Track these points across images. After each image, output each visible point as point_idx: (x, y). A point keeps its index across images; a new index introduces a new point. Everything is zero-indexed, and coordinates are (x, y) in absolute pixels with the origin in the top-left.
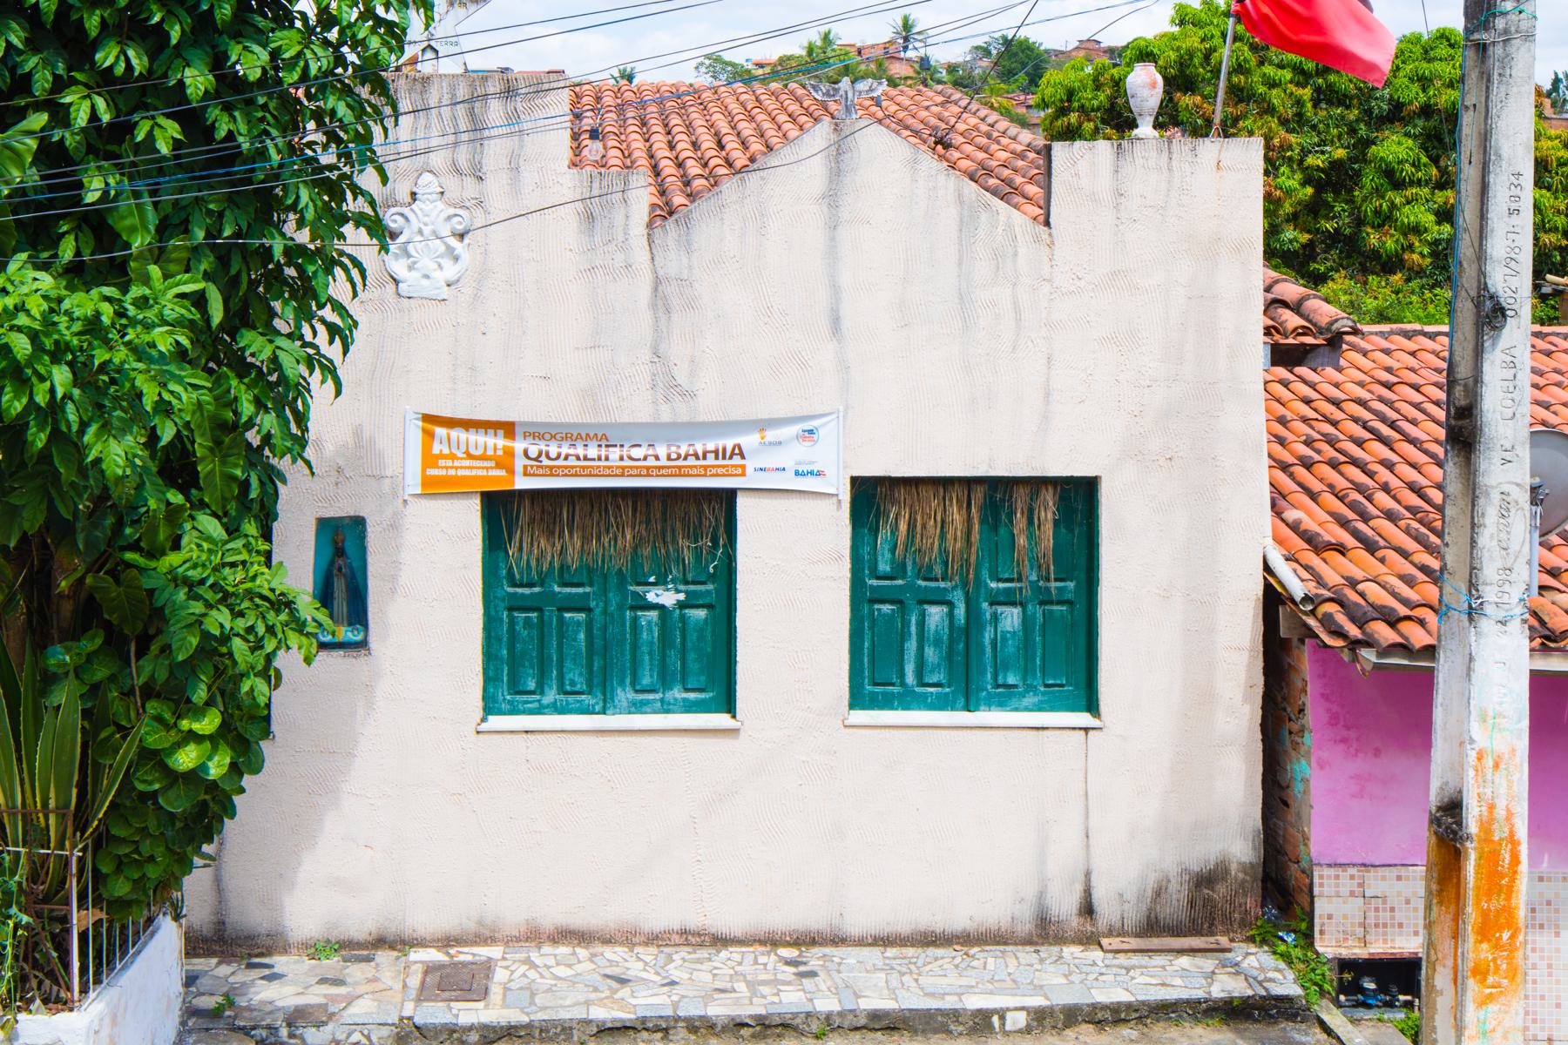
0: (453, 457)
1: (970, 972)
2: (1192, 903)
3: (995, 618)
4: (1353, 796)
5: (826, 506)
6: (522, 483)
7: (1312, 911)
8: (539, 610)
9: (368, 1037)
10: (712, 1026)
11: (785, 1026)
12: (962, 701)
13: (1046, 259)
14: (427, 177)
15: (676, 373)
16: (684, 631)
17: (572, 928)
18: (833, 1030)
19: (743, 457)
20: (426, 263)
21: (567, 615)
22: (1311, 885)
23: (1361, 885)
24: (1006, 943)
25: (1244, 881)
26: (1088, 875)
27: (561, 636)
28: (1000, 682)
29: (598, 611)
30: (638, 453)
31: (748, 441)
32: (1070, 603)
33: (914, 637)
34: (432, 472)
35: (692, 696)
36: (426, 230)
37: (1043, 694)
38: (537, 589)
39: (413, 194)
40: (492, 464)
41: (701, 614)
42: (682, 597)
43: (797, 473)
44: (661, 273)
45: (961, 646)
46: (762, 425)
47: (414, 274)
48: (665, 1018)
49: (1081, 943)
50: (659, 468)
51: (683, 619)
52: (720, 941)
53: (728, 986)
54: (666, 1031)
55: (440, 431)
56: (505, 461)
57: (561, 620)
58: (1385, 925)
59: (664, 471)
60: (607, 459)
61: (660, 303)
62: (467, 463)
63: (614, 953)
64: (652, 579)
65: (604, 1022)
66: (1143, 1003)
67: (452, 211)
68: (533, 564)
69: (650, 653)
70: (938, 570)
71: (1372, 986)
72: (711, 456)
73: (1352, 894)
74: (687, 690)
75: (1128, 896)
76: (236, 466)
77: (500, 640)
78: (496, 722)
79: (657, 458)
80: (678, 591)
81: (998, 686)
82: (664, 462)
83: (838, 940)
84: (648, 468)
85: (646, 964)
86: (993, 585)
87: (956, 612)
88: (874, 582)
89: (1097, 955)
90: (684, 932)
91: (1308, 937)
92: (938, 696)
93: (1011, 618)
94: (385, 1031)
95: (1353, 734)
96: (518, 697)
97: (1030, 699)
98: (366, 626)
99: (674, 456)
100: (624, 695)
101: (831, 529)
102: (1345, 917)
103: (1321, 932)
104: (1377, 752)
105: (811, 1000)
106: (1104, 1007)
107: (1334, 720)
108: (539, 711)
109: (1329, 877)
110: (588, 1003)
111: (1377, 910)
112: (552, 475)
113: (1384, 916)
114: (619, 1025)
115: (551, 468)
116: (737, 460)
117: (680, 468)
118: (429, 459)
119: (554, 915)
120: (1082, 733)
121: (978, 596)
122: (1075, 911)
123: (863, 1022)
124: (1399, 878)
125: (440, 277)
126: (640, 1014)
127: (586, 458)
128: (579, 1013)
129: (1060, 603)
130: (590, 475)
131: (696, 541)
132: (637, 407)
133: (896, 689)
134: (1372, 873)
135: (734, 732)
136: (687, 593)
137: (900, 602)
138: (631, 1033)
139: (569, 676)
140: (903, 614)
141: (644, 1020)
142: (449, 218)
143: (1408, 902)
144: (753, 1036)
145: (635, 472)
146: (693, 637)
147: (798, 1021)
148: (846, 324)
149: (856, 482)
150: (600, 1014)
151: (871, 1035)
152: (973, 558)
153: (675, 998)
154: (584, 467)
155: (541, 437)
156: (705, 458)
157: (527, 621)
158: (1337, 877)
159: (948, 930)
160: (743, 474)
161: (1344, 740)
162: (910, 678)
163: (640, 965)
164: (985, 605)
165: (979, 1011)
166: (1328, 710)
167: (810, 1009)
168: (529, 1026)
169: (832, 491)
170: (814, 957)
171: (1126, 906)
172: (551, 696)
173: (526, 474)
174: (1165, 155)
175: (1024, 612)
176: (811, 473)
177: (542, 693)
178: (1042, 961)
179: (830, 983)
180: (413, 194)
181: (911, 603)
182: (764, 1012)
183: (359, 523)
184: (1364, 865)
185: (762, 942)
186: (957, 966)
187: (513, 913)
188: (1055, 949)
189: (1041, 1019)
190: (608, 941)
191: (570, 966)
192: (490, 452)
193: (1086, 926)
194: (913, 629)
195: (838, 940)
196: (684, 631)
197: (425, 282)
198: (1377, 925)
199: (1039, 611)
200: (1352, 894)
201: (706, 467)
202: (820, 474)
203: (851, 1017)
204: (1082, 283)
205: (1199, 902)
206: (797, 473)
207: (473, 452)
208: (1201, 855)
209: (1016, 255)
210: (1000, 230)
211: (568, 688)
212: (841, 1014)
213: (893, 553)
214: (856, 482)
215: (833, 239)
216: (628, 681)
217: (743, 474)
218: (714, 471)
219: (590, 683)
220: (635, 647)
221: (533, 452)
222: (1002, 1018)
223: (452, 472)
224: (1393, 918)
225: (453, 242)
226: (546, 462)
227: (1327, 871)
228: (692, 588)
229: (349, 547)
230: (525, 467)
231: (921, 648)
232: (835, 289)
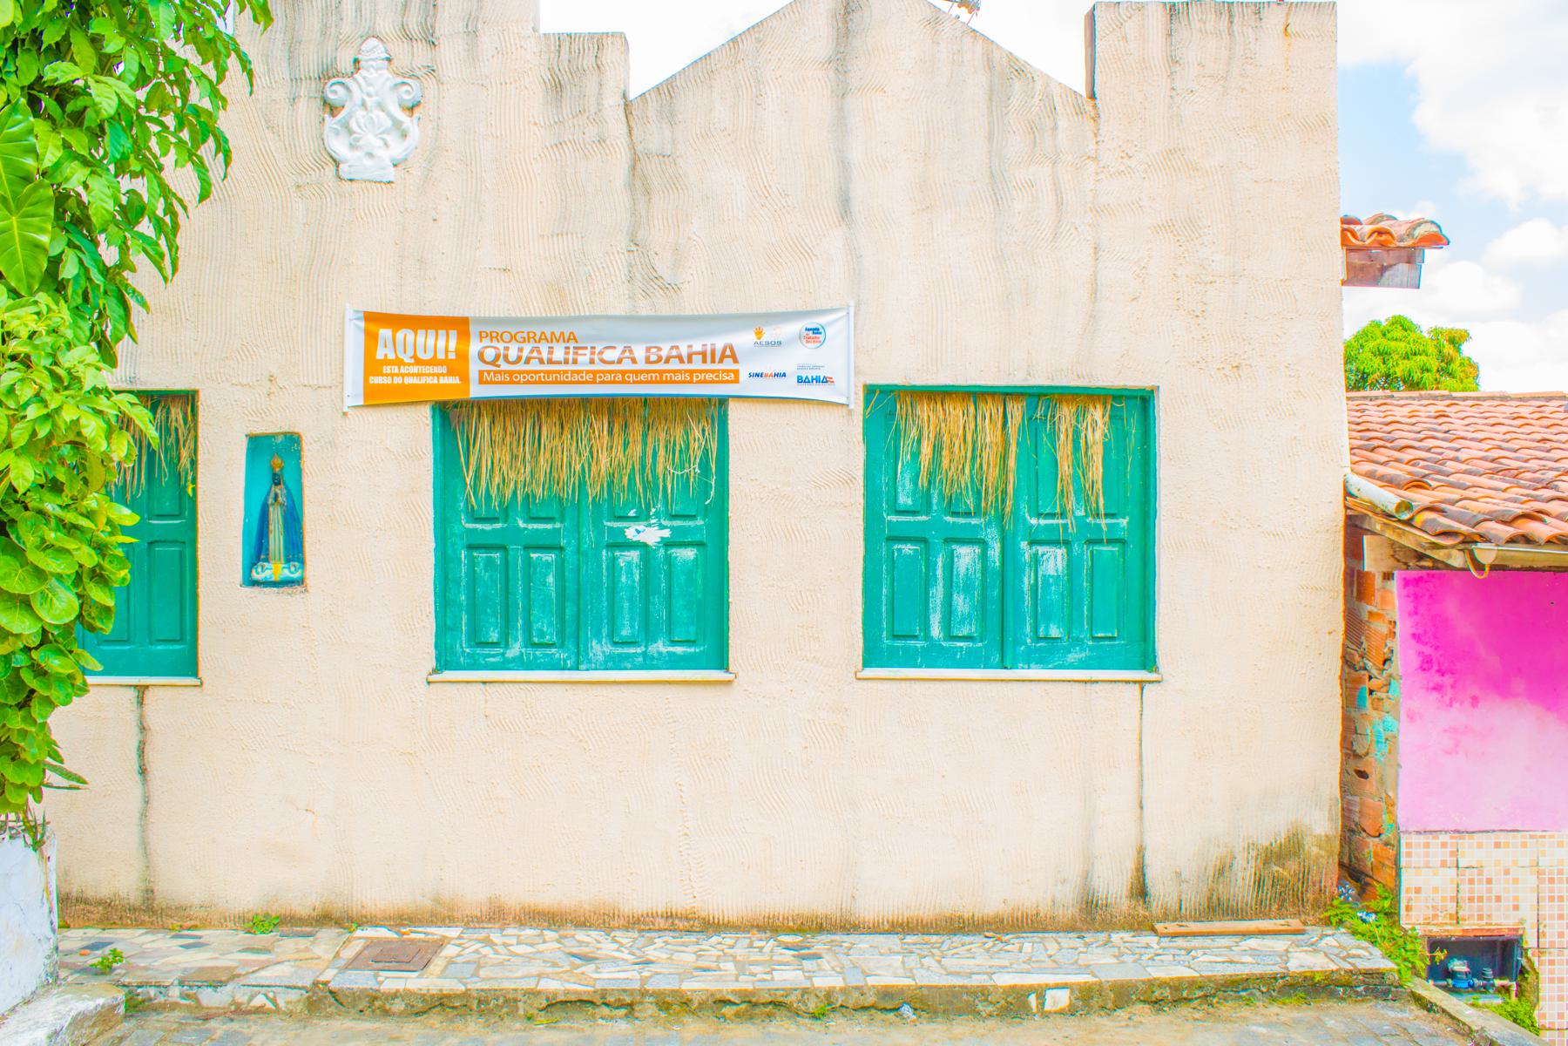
0: (400, 363)
1: (1003, 954)
2: (1259, 883)
3: (1036, 560)
4: (1447, 752)
5: (832, 418)
6: (476, 391)
7: (1398, 886)
8: (503, 548)
9: (274, 1001)
10: (686, 1003)
11: (777, 1004)
13: (1090, 135)
14: (373, 42)
15: (657, 264)
16: (669, 575)
17: (540, 908)
18: (834, 1010)
19: (736, 361)
20: (371, 140)
21: (534, 556)
22: (1398, 855)
23: (1455, 854)
24: (1045, 930)
25: (1318, 857)
26: (1141, 851)
27: (528, 579)
29: (569, 550)
30: (610, 355)
31: (743, 340)
32: (1122, 542)
33: (940, 582)
34: (375, 380)
35: (679, 650)
36: (370, 102)
37: (1091, 649)
38: (498, 526)
39: (357, 61)
40: (443, 370)
41: (689, 554)
42: (666, 533)
43: (800, 380)
44: (639, 148)
45: (996, 593)
47: (358, 153)
48: (631, 992)
49: (1131, 929)
50: (636, 372)
51: (669, 560)
53: (714, 965)
54: (631, 1006)
55: (385, 333)
56: (458, 366)
57: (528, 563)
58: (1480, 899)
59: (642, 377)
60: (575, 362)
61: (638, 184)
62: (415, 369)
63: (588, 938)
64: (632, 513)
65: (555, 994)
67: (399, 80)
68: (494, 493)
69: (630, 600)
70: (970, 502)
71: (1464, 969)
72: (697, 359)
73: (1444, 864)
74: (673, 643)
75: (1185, 875)
76: (42, 230)
77: (458, 583)
78: (449, 675)
79: (634, 361)
80: (662, 527)
81: (1039, 639)
82: (642, 365)
83: (850, 927)
84: (624, 373)
85: (622, 945)
86: (1034, 521)
88: (894, 518)
89: (1152, 940)
90: (669, 916)
91: (1392, 915)
92: (969, 650)
93: (1054, 561)
94: (294, 995)
95: (1448, 680)
96: (478, 650)
98: (303, 562)
100: (599, 648)
101: (841, 445)
102: (1436, 890)
103: (1408, 908)
104: (1475, 701)
105: (810, 978)
107: (1426, 664)
108: (504, 665)
109: (1418, 845)
110: (540, 976)
111: (1471, 881)
112: (511, 382)
113: (1480, 889)
114: (573, 998)
115: (511, 373)
116: (728, 364)
117: (661, 372)
118: (372, 366)
119: (521, 891)
121: (1014, 535)
122: (1125, 891)
123: (870, 999)
124: (1497, 845)
125: (385, 155)
126: (599, 986)
127: (550, 361)
128: (530, 984)
129: (1110, 542)
130: (556, 382)
131: (683, 468)
132: (614, 299)
133: (919, 644)
134: (1467, 841)
135: (729, 682)
136: (672, 528)
137: (924, 540)
138: (590, 1009)
139: (536, 626)
140: (927, 554)
141: (604, 993)
142: (396, 86)
143: (1507, 872)
144: (737, 1015)
145: (609, 377)
146: (680, 580)
147: (792, 998)
149: (870, 391)
150: (551, 985)
151: (879, 1016)
152: (1010, 488)
153: (646, 974)
154: (548, 373)
155: (498, 337)
156: (690, 361)
157: (489, 563)
158: (1427, 845)
160: (736, 381)
161: (1437, 688)
162: (936, 631)
163: (616, 946)
164: (1024, 545)
166: (1421, 653)
167: (807, 984)
168: (466, 995)
169: (842, 400)
170: (820, 943)
171: (1184, 886)
172: (516, 649)
173: (481, 382)
174: (1225, 18)
175: (1069, 553)
176: (817, 380)
177: (507, 646)
178: (1087, 945)
179: (834, 963)
180: (357, 61)
181: (937, 541)
182: (750, 987)
183: (293, 441)
185: (760, 928)
186: (988, 950)
187: (473, 892)
188: (1103, 936)
190: (583, 924)
191: (532, 945)
192: (441, 356)
193: (1140, 909)
194: (939, 572)
195: (850, 927)
196: (669, 575)
197: (368, 162)
198: (1471, 899)
199: (1086, 552)
200: (1444, 864)
201: (691, 372)
202: (826, 380)
203: (857, 994)
204: (1133, 163)
206: (800, 380)
207: (421, 356)
208: (1269, 828)
209: (1055, 128)
210: (1036, 99)
211: (536, 640)
212: (844, 991)
213: (916, 484)
214: (870, 391)
215: (841, 109)
216: (605, 631)
217: (736, 381)
218: (701, 377)
219: (561, 633)
220: (613, 592)
221: (490, 354)
223: (398, 380)
224: (1489, 891)
225: (402, 116)
226: (504, 366)
227: (1415, 839)
229: (288, 477)
230: (481, 373)
232: (844, 165)
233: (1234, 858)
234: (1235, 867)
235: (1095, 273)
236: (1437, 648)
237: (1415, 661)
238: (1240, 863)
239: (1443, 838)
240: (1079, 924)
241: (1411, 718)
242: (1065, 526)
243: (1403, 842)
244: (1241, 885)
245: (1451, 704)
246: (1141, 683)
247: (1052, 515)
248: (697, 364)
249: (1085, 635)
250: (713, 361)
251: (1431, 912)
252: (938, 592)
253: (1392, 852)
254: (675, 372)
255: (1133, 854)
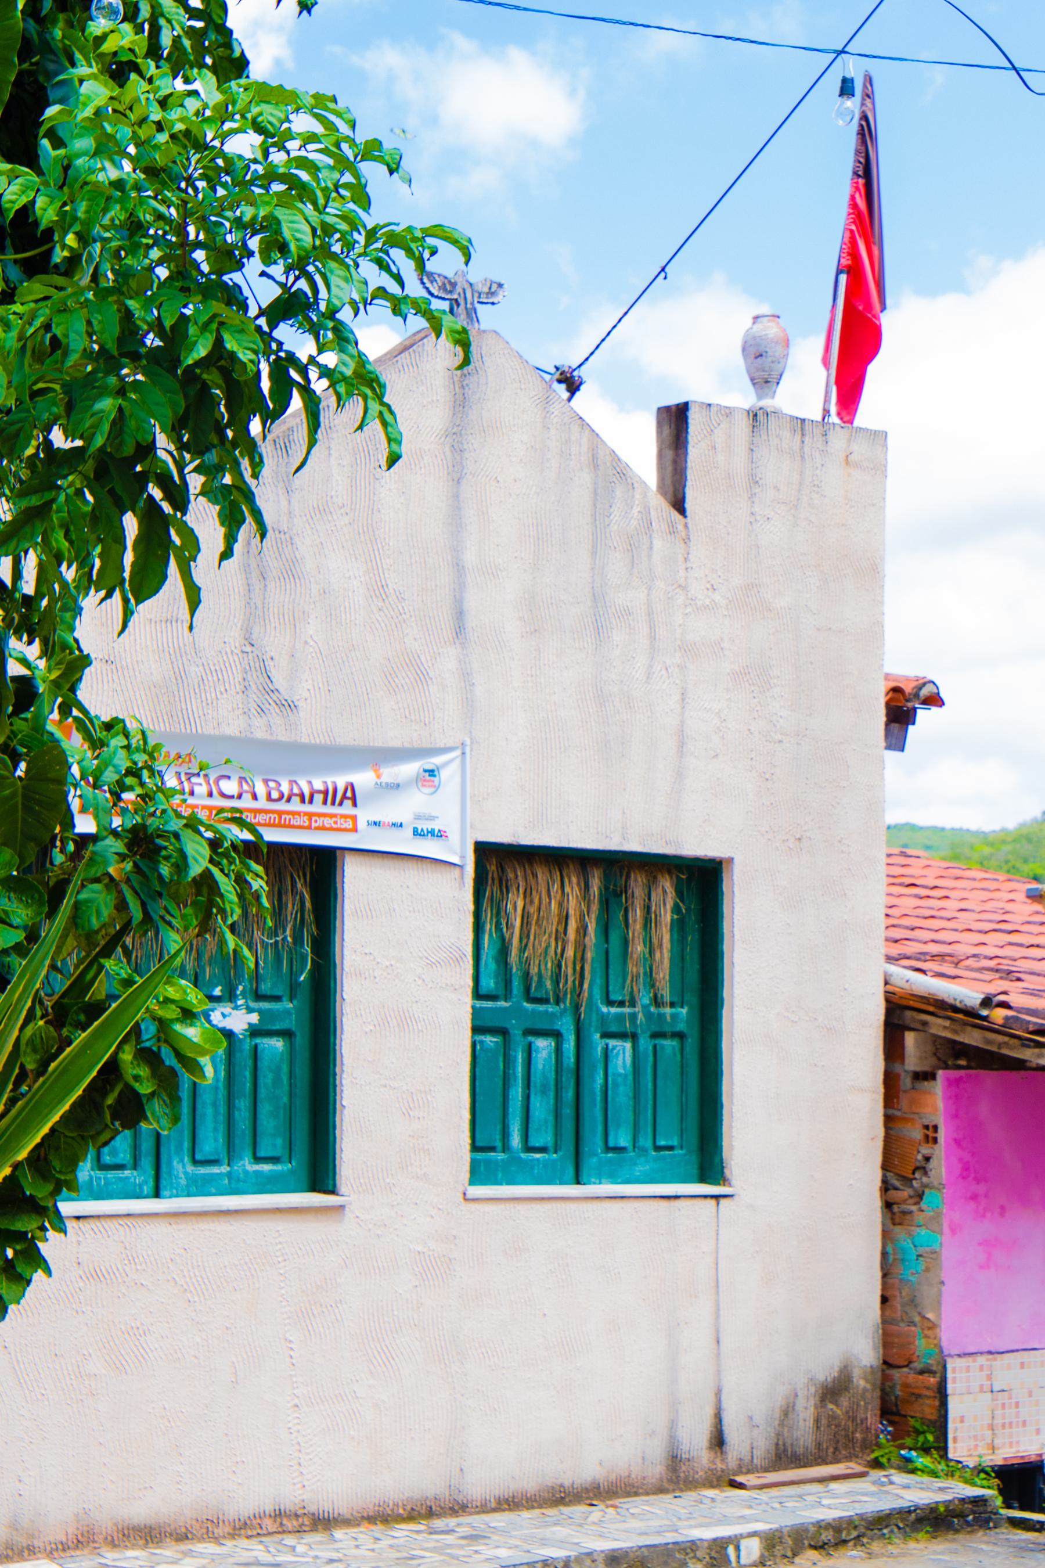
4: (982, 1267)
12: (570, 1171)
13: (681, 559)
15: (273, 674)
19: (355, 805)
23: (989, 1377)
24: (636, 1494)
25: (865, 1390)
26: (718, 1393)
28: (611, 1144)
30: (230, 787)
31: (363, 779)
32: (680, 1036)
35: (266, 1168)
41: (278, 1044)
42: (254, 1018)
46: (378, 757)
49: (712, 1486)
52: (323, 1522)
66: (861, 1516)
69: (215, 1105)
73: (982, 1390)
75: (758, 1419)
79: (255, 797)
80: (250, 1010)
82: (262, 803)
83: (458, 1508)
87: (565, 1046)
90: (278, 1515)
92: (546, 1164)
95: (981, 1189)
97: (642, 1167)
99: (275, 795)
103: (955, 1440)
106: (828, 1526)
107: (966, 1171)
116: (347, 808)
117: (280, 813)
120: (713, 1202)
124: (1022, 1365)
136: (260, 1012)
143: (1030, 1395)
148: (471, 622)
158: (968, 1369)
159: (578, 1483)
161: (974, 1197)
162: (516, 1141)
165: (715, 1540)
166: (961, 1160)
169: (455, 860)
174: (798, 437)
175: (635, 1048)
176: (432, 832)
181: (516, 1033)
184: (990, 1353)
185: (371, 1519)
189: (771, 1541)
198: (1003, 1426)
200: (982, 1390)
201: (310, 815)
202: (441, 835)
204: (717, 597)
205: (824, 1421)
206: (416, 833)
208: (824, 1367)
210: (635, 510)
214: (484, 851)
215: (456, 497)
222: (738, 1548)
224: (1017, 1415)
228: (265, 1005)
231: (527, 1098)
232: (459, 569)
233: (796, 1395)
234: (797, 1408)
235: (682, 722)
236: (973, 1154)
237: (958, 1168)
238: (801, 1403)
239: (981, 1360)
240: (666, 1485)
241: (953, 1231)
242: (633, 1017)
243: (949, 1366)
244: (804, 1431)
245: (984, 1216)
246: (717, 1197)
247: (621, 1004)
248: (317, 807)
249: (646, 1142)
250: (333, 803)
251: (972, 1443)
252: (517, 1092)
253: (933, 1380)
254: (294, 813)
255: (711, 1398)
